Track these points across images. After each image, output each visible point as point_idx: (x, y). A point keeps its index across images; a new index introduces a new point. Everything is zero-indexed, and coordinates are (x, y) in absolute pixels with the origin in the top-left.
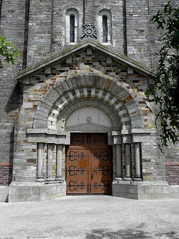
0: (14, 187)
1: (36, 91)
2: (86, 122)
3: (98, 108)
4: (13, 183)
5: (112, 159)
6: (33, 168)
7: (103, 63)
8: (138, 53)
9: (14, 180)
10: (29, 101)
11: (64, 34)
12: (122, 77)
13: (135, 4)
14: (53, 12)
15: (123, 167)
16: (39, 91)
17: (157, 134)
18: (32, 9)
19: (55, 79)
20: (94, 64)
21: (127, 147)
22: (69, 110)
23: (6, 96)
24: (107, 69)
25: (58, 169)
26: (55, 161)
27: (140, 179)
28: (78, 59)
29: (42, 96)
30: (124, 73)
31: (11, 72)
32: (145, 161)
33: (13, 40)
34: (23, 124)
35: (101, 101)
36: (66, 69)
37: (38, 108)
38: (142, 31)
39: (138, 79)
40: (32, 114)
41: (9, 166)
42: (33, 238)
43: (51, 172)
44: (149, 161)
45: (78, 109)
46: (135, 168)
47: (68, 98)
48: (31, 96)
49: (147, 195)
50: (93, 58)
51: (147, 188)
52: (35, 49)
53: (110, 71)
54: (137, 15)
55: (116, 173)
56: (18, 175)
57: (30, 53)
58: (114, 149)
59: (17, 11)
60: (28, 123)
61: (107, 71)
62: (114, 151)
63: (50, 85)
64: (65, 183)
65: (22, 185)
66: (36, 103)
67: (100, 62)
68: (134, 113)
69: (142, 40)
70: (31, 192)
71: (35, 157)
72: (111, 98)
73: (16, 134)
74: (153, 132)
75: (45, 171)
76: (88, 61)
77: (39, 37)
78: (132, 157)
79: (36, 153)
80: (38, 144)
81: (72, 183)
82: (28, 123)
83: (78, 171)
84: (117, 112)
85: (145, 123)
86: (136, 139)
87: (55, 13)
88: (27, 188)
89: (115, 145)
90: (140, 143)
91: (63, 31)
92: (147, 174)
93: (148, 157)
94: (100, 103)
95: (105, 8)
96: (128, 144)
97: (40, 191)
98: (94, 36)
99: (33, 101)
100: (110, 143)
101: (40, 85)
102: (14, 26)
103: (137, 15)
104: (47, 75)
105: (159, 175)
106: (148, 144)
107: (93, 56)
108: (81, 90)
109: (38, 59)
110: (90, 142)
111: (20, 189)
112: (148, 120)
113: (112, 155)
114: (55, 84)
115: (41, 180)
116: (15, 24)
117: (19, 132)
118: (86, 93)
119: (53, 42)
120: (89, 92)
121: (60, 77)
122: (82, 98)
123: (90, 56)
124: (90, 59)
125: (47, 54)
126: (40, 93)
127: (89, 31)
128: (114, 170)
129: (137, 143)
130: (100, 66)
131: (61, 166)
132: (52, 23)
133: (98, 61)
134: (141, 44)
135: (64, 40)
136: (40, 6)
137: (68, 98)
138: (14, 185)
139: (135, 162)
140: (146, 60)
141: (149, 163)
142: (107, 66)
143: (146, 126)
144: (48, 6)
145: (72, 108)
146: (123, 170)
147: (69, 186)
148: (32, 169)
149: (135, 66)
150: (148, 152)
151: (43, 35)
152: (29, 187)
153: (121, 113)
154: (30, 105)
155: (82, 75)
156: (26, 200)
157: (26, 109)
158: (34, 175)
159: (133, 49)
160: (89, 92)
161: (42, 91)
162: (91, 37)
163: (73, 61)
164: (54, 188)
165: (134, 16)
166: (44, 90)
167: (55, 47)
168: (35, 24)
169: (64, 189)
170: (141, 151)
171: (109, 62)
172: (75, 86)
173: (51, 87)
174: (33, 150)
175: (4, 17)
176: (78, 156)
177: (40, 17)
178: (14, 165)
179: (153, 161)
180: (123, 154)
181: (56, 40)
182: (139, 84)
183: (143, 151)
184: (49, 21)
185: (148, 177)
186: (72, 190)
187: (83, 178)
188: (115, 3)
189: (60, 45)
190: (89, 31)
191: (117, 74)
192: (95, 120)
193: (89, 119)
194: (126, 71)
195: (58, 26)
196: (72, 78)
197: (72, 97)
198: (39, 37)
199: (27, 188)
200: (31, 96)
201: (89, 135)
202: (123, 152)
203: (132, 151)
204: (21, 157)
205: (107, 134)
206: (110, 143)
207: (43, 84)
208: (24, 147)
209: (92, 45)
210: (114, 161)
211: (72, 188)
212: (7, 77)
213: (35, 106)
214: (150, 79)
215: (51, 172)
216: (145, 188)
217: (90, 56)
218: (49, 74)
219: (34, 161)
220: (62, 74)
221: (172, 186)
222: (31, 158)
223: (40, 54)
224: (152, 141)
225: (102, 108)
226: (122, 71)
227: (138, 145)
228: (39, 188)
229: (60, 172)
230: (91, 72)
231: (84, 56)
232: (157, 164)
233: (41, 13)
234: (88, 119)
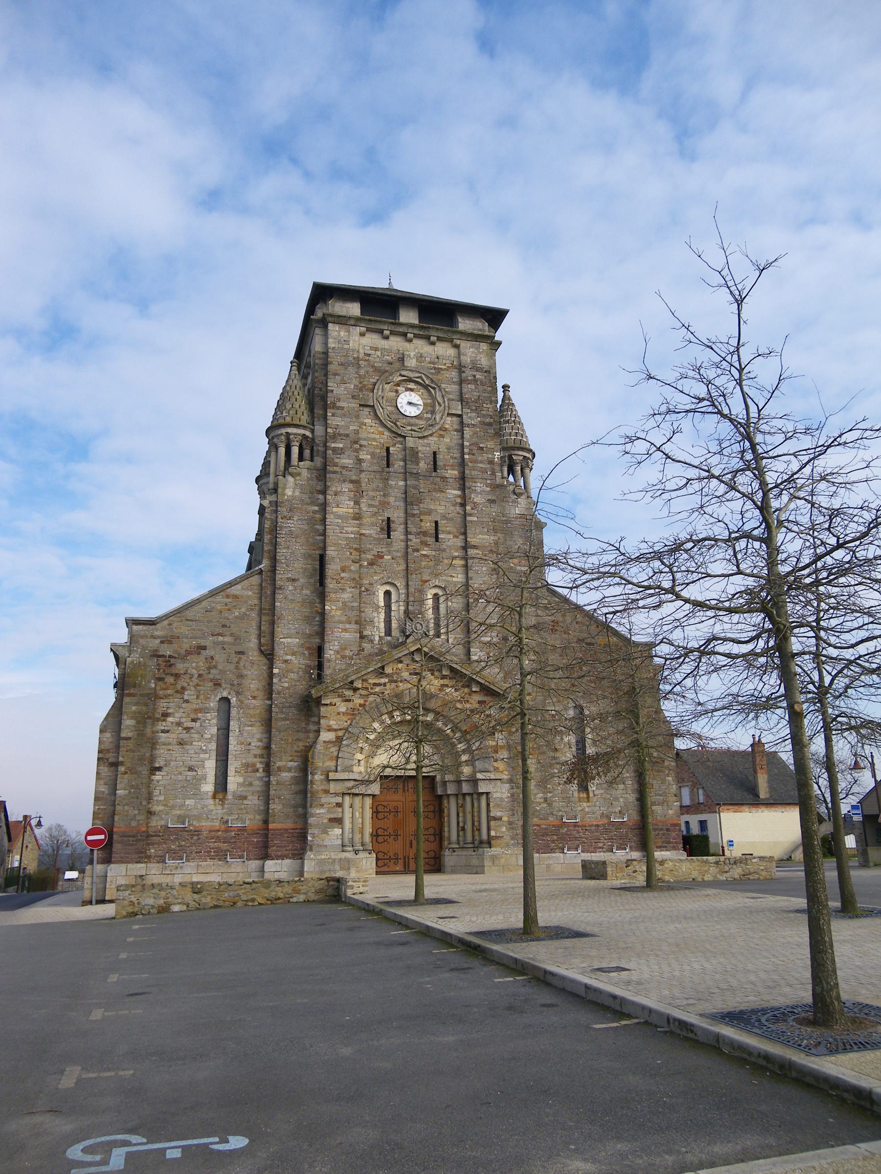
0: (312, 859)
6: (338, 831)
7: (436, 673)
9: (311, 850)
10: (329, 730)
15: (460, 829)
17: (510, 781)
18: (330, 585)
21: (468, 799)
23: (288, 720)
25: (364, 834)
27: (487, 846)
28: (400, 666)
30: (466, 690)
31: (295, 681)
32: (495, 819)
33: (296, 628)
34: (320, 765)
36: (383, 680)
39: (485, 699)
41: (301, 829)
44: (500, 819)
46: (479, 830)
48: (332, 723)
49: (496, 868)
51: (497, 858)
52: (336, 648)
53: (447, 686)
55: (449, 838)
56: (318, 841)
57: (329, 653)
63: (360, 705)
65: (323, 857)
71: (340, 816)
73: (311, 781)
74: (505, 777)
77: (342, 629)
83: (390, 835)
87: (363, 589)
88: (331, 860)
90: (487, 794)
92: (496, 837)
93: (499, 814)
95: (437, 583)
96: (468, 794)
97: (349, 864)
99: (335, 730)
101: (344, 706)
102: (297, 605)
105: (512, 838)
109: (340, 665)
110: (408, 790)
114: (367, 703)
116: (298, 602)
117: (316, 777)
119: (362, 637)
128: (446, 834)
129: (483, 793)
136: (342, 578)
139: (479, 821)
141: (498, 823)
143: (496, 769)
146: (461, 833)
148: (337, 833)
149: (483, 682)
150: (498, 805)
151: (348, 626)
152: (334, 860)
157: (325, 742)
170: (488, 805)
173: (361, 708)
174: (337, 804)
175: (280, 589)
176: (390, 812)
177: (342, 596)
178: (309, 827)
179: (505, 819)
181: (365, 633)
184: (356, 604)
185: (498, 841)
187: (395, 847)
188: (451, 576)
189: (372, 641)
191: (456, 690)
198: (342, 629)
199: (331, 860)
200: (333, 723)
203: (476, 805)
204: (319, 814)
208: (323, 800)
212: (288, 688)
216: (494, 858)
219: (339, 821)
222: (335, 816)
225: (264, 618)
227: (484, 796)
228: (348, 861)
229: (367, 839)
232: (510, 823)
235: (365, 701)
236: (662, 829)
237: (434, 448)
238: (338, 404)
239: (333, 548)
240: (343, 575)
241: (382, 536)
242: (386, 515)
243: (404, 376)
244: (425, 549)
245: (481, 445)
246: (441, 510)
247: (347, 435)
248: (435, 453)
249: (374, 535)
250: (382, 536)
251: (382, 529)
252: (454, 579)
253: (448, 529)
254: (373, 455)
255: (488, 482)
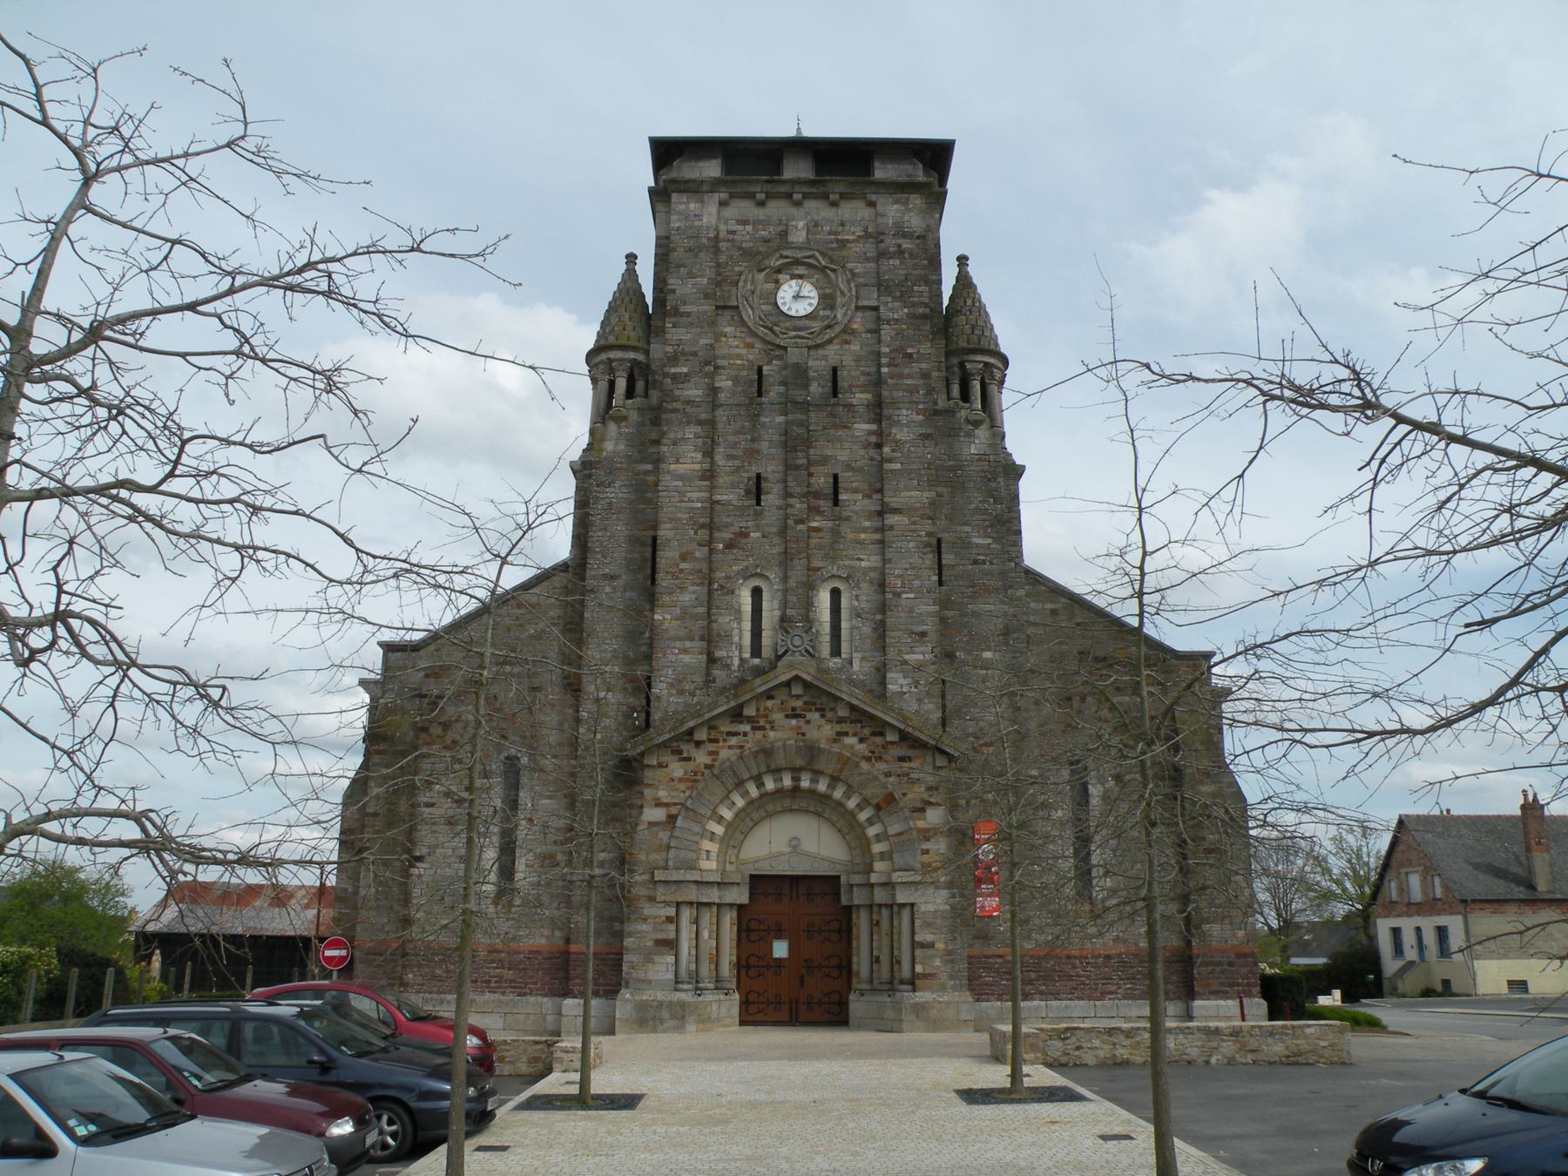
0: (628, 1000)
1: (673, 780)
2: (789, 849)
3: (819, 815)
4: (626, 994)
5: (849, 941)
7: (829, 715)
8: (913, 689)
9: (627, 986)
11: (736, 639)
12: (872, 748)
13: (907, 566)
14: (710, 584)
16: (680, 780)
18: (664, 581)
19: (715, 753)
20: (809, 716)
22: (748, 820)
24: (838, 728)
26: (714, 943)
27: (909, 987)
28: (769, 703)
29: (687, 793)
30: (878, 740)
32: (923, 945)
35: (825, 798)
37: (679, 822)
38: (923, 634)
39: (910, 753)
40: (664, 836)
42: (1395, 156)
43: (706, 970)
44: (931, 945)
45: (769, 815)
46: (899, 962)
47: (745, 794)
50: (805, 703)
53: (846, 734)
54: (912, 596)
55: (858, 974)
57: (659, 688)
58: (854, 916)
59: (624, 577)
60: (654, 857)
61: (840, 734)
62: (854, 921)
63: (706, 766)
64: (737, 996)
66: (674, 811)
67: (822, 711)
68: (900, 834)
69: (921, 657)
70: (665, 1014)
71: (672, 935)
72: (847, 796)
75: (693, 967)
76: (794, 709)
78: (895, 937)
79: (672, 927)
80: (678, 904)
81: (752, 997)
82: (654, 857)
84: (862, 828)
85: (925, 858)
86: (902, 897)
87: (716, 586)
89: (858, 907)
90: (912, 905)
91: (736, 632)
92: (925, 976)
93: (929, 938)
94: (819, 805)
95: (835, 572)
96: (886, 905)
98: (807, 651)
99: (667, 805)
100: (844, 901)
103: (912, 596)
104: (698, 744)
105: (952, 978)
106: (931, 908)
107: (806, 698)
108: (777, 776)
111: (641, 1007)
112: (931, 852)
113: (850, 931)
115: (685, 987)
118: (787, 782)
119: (712, 660)
120: (796, 779)
121: (730, 747)
122: (779, 792)
123: (798, 697)
124: (799, 704)
125: (698, 692)
126: (682, 786)
127: (797, 641)
128: (855, 967)
129: (903, 905)
130: (822, 721)
131: (728, 956)
132: (709, 613)
133: (817, 710)
134: (919, 668)
135: (737, 653)
136: (681, 571)
137: (745, 794)
138: (628, 996)
140: (931, 706)
141: (930, 952)
142: (838, 722)
144: (700, 571)
145: (755, 815)
147: (745, 1004)
151: (688, 644)
152: (661, 1003)
153: (872, 831)
154: (659, 814)
155: (780, 744)
156: (654, 1030)
157: (650, 823)
158: (671, 976)
159: (902, 681)
160: (796, 779)
161: (686, 780)
162: (802, 655)
163: (758, 710)
164: (714, 1007)
165: (904, 596)
166: (692, 780)
167: (718, 673)
168: (669, 617)
169: (736, 1011)
171: (843, 712)
172: (763, 769)
173: (707, 771)
179: (940, 946)
180: (875, 929)
181: (718, 654)
182: (912, 765)
183: (917, 923)
186: (751, 1016)
189: (728, 667)
190: (797, 641)
192: (809, 845)
193: (795, 844)
194: (882, 734)
195: (724, 620)
196: (756, 752)
197: (754, 792)
200: (663, 794)
201: (795, 880)
202: (874, 924)
203: (895, 923)
204: (640, 934)
205: (839, 877)
206: (844, 901)
207: (690, 766)
209: (804, 676)
210: (854, 944)
211: (752, 1009)
213: (672, 818)
214: (937, 755)
215: (706, 970)
216: (919, 1009)
217: (798, 697)
218: (703, 742)
220: (734, 741)
221: (984, 1004)
223: (681, 692)
224: (939, 901)
226: (874, 734)
228: (682, 1005)
229: (726, 970)
230: (800, 737)
231: (784, 697)
232: (949, 953)
233: (682, 589)
234: (794, 843)
235: (714, 760)
236: (1220, 963)
237: (833, 362)
238: (683, 309)
239: (668, 526)
240: (683, 565)
241: (747, 503)
242: (755, 469)
243: (787, 257)
244: (817, 518)
245: (909, 351)
246: (843, 456)
247: (695, 354)
248: (835, 370)
249: (735, 502)
250: (747, 503)
251: (748, 492)
252: (863, 564)
253: (854, 485)
254: (736, 380)
255: (921, 406)
